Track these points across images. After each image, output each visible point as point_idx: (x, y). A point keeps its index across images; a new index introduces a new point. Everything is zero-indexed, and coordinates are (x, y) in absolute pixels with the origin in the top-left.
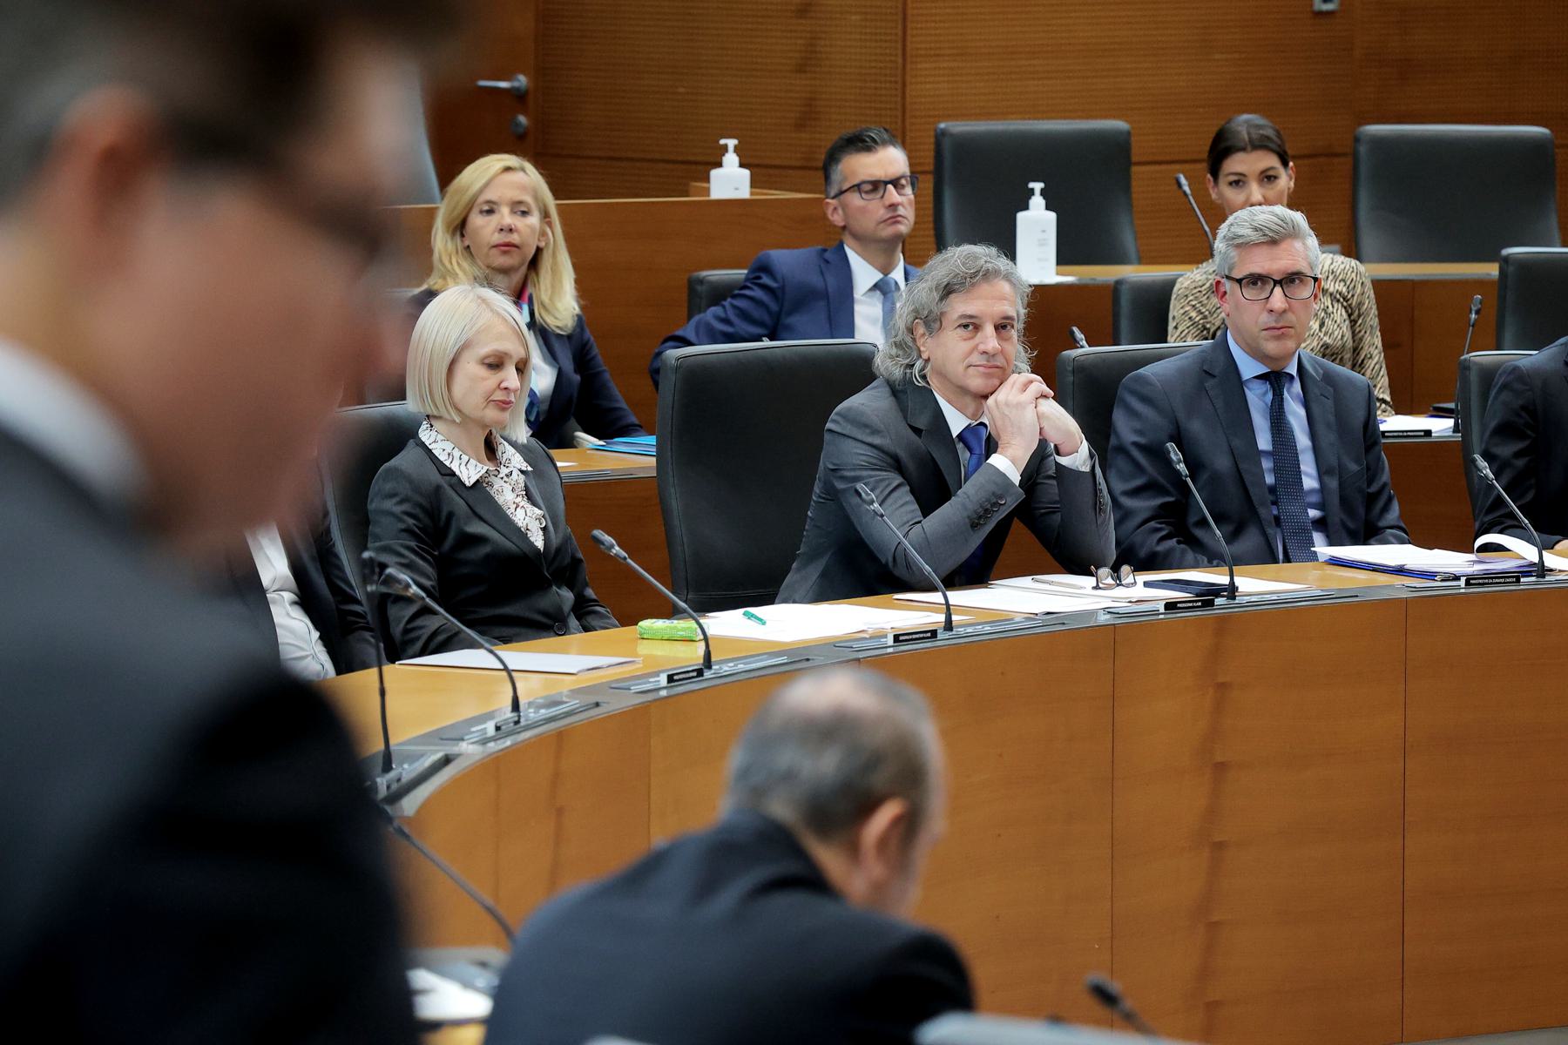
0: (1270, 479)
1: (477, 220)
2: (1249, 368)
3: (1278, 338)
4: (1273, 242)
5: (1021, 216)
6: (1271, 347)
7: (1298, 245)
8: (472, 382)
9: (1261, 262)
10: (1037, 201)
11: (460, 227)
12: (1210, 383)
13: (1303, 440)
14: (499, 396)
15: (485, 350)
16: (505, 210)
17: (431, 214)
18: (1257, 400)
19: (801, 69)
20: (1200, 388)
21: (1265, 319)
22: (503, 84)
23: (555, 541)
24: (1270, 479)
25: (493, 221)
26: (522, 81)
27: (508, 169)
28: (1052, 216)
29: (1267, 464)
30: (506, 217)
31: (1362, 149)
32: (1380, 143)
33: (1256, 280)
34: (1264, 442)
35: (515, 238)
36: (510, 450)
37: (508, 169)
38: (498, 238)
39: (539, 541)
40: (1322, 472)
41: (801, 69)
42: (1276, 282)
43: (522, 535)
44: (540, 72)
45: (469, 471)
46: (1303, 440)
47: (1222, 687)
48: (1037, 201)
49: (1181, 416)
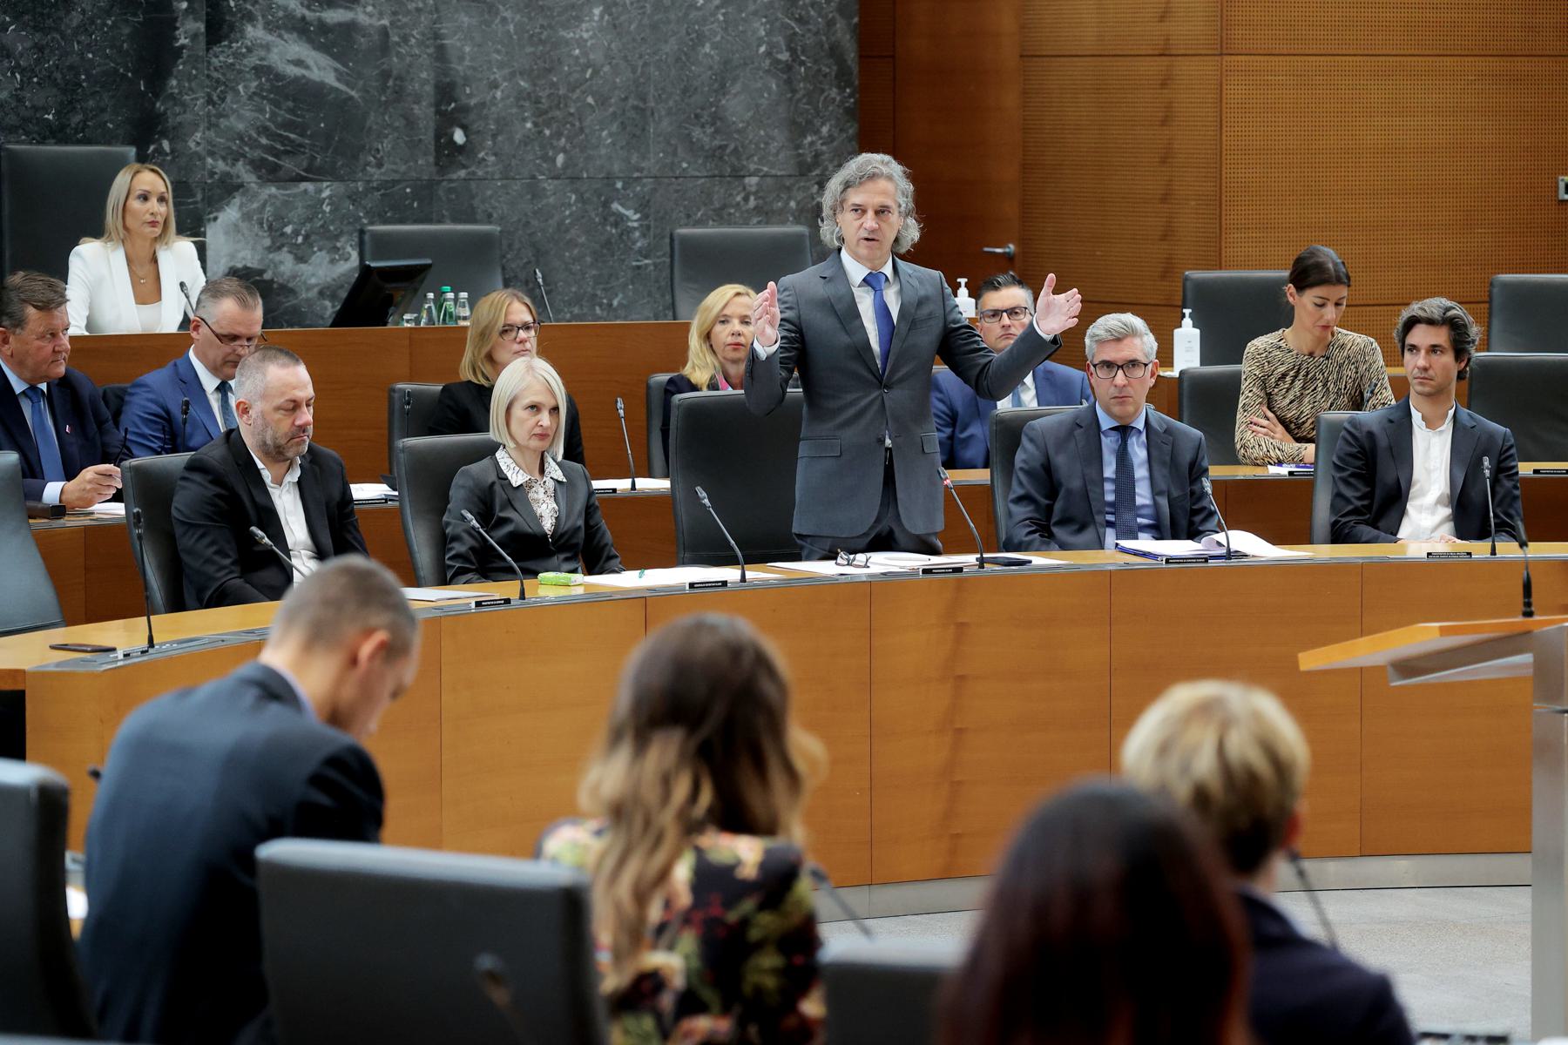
0: (1110, 497)
1: (718, 328)
2: (1106, 423)
3: (1122, 404)
4: (1118, 340)
5: (1177, 331)
6: (1116, 409)
7: (1137, 341)
8: (523, 422)
9: (1111, 354)
10: (1187, 322)
11: (707, 337)
12: (1078, 432)
13: (1141, 472)
14: (538, 430)
15: (527, 401)
16: (736, 322)
17: (687, 327)
18: (1109, 444)
19: (1164, 237)
20: (1070, 434)
21: (1113, 391)
22: (999, 250)
23: (565, 527)
24: (1110, 497)
25: (728, 328)
26: (1012, 248)
27: (738, 294)
28: (1197, 331)
29: (1109, 487)
30: (736, 325)
31: (1495, 290)
32: (1506, 286)
33: (1109, 365)
34: (1109, 471)
35: (742, 340)
36: (553, 464)
37: (738, 294)
38: (730, 340)
39: (548, 525)
40: (1155, 492)
41: (1164, 237)
42: (1121, 367)
43: (538, 519)
44: (1023, 242)
45: (517, 478)
46: (1141, 472)
47: (962, 625)
48: (1187, 322)
49: (1051, 452)
